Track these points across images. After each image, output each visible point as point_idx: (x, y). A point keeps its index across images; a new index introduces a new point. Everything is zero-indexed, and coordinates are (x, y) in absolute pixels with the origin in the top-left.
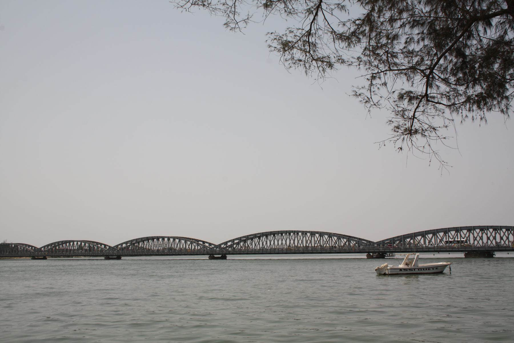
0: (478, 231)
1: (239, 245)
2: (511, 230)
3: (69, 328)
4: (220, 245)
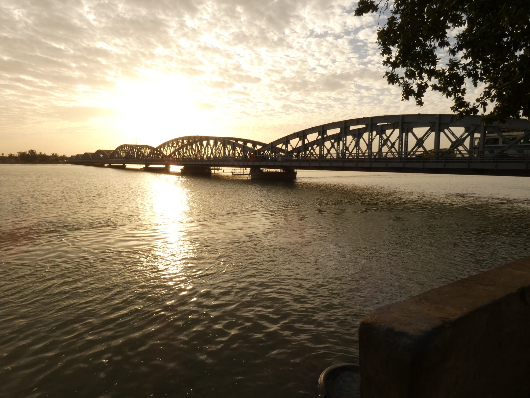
1: (341, 143)
3: (203, 72)
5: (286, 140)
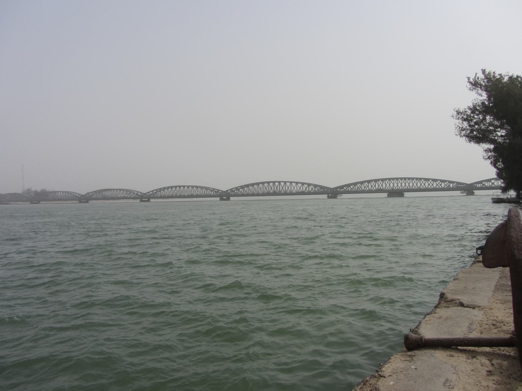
0: (380, 181)
2: (411, 180)
4: (146, 193)
5: (149, 192)
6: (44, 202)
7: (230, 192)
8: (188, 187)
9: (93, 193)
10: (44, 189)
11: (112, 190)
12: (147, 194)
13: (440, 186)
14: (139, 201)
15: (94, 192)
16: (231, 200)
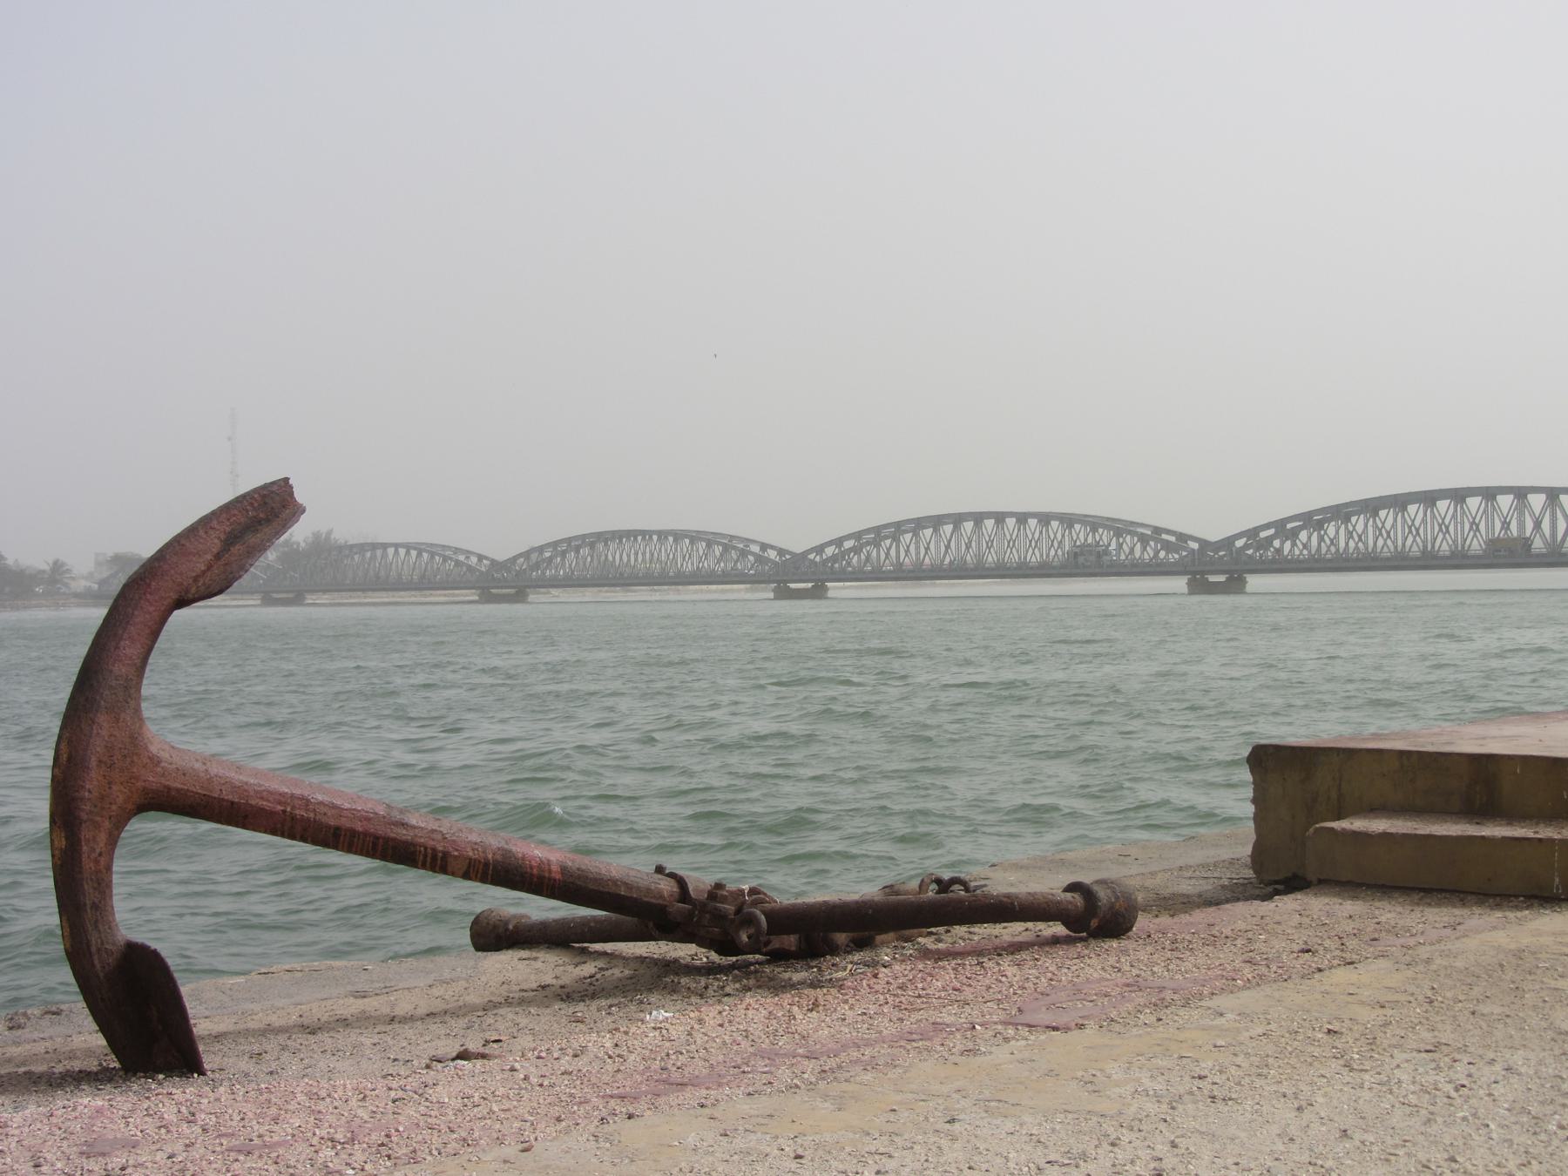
5: (819, 549)
6: (324, 598)
7: (1246, 546)
8: (1022, 518)
9: (547, 555)
10: (324, 530)
11: (640, 538)
12: (811, 556)
13: (1305, 552)
14: (771, 595)
15: (548, 545)
16: (1249, 588)
